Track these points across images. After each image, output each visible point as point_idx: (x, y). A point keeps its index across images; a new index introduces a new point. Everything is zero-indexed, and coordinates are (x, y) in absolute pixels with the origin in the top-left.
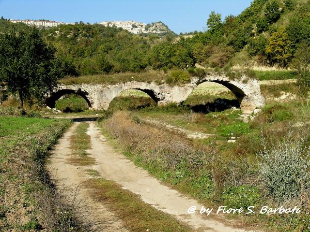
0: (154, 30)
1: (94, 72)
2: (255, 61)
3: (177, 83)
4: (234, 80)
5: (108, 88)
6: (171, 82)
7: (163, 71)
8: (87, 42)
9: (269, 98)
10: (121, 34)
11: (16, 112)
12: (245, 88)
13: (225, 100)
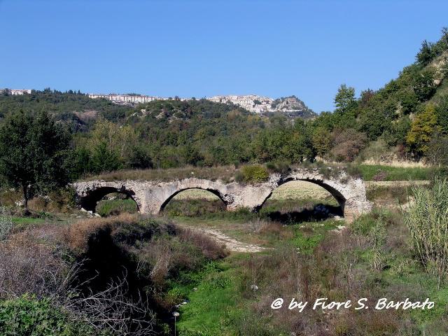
0: (284, 107)
1: (175, 164)
2: (395, 153)
3: (250, 181)
4: (329, 179)
5: (159, 186)
6: (243, 180)
7: (233, 165)
8: (182, 125)
9: (391, 205)
10: (231, 113)
11: (18, 211)
12: (345, 191)
13: (328, 207)
